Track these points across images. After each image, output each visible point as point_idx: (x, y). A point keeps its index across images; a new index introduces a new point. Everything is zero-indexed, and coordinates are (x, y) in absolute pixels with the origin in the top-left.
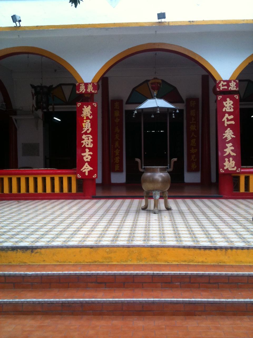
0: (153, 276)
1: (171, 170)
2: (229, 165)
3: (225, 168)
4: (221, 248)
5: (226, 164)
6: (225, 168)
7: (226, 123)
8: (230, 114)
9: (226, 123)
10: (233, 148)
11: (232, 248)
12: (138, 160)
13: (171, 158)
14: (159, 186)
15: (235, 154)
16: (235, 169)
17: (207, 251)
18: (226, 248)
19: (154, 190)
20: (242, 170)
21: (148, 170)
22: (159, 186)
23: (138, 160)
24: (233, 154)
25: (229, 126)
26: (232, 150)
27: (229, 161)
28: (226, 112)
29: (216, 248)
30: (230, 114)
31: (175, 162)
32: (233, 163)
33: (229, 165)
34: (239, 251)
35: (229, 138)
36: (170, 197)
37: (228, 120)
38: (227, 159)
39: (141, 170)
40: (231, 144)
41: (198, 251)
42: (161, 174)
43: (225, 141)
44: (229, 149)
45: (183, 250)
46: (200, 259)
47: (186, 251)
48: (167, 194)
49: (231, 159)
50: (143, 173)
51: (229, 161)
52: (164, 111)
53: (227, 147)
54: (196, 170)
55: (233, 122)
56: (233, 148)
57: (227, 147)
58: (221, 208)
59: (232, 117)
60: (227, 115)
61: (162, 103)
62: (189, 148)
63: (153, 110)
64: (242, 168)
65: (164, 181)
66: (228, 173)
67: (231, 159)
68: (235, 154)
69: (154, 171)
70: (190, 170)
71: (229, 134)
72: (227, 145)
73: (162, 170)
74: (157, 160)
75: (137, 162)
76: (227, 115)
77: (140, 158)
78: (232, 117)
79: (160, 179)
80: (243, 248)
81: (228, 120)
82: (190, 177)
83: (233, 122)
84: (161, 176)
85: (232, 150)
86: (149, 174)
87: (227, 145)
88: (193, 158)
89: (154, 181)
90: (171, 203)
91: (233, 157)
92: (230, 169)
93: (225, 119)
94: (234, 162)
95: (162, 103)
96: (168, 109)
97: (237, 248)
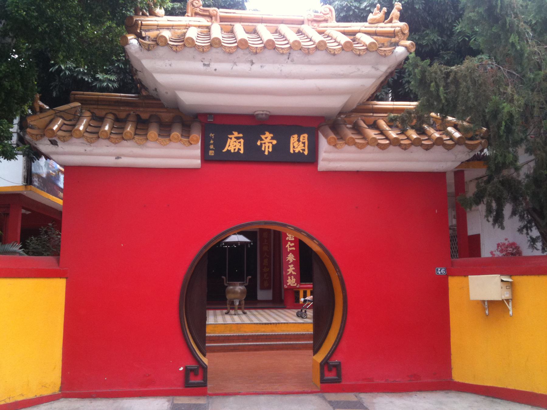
0: (239, 336)
1: (247, 284)
2: (291, 282)
3: (288, 284)
4: (273, 323)
5: (289, 281)
6: (288, 284)
7: (289, 249)
8: (292, 242)
9: (289, 249)
10: (294, 269)
11: (279, 323)
12: (224, 277)
13: (247, 276)
14: (239, 295)
15: (295, 273)
16: (295, 285)
17: (267, 325)
18: (276, 324)
19: (234, 299)
20: (301, 286)
21: (230, 285)
22: (239, 295)
23: (224, 277)
24: (294, 273)
25: (291, 251)
26: (293, 270)
27: (291, 278)
28: (288, 241)
29: (271, 324)
30: (292, 242)
31: (250, 279)
32: (294, 280)
33: (291, 282)
34: (283, 325)
35: (291, 261)
36: (246, 308)
37: (290, 247)
38: (289, 277)
39: (226, 285)
40: (292, 265)
41: (262, 326)
42: (240, 287)
43: (288, 263)
44: (291, 269)
45: (254, 325)
46: (263, 330)
47: (256, 326)
48: (243, 306)
49: (292, 277)
50: (227, 287)
51: (291, 278)
52: (243, 243)
53: (289, 268)
54: (268, 288)
55: (294, 249)
56: (294, 269)
57: (289, 268)
58: (285, 315)
59: (293, 244)
60: (289, 243)
61: (242, 238)
62: (262, 267)
63: (236, 243)
64: (300, 285)
65: (242, 292)
66: (291, 288)
67: (292, 277)
68: (295, 273)
69: (235, 285)
70: (262, 288)
71: (291, 258)
72: (289, 266)
73: (241, 285)
74: (237, 277)
75: (223, 279)
76: (289, 243)
77: (225, 276)
78: (293, 244)
79: (239, 291)
80: (285, 323)
81: (290, 247)
82: (263, 295)
83: (294, 249)
84: (240, 289)
85: (293, 270)
86: (231, 287)
87: (289, 266)
88: (265, 276)
89: (235, 292)
90: (246, 311)
91: (294, 275)
92: (292, 285)
93: (288, 246)
94: (294, 280)
95: (242, 238)
96: (245, 242)
97: (282, 323)
